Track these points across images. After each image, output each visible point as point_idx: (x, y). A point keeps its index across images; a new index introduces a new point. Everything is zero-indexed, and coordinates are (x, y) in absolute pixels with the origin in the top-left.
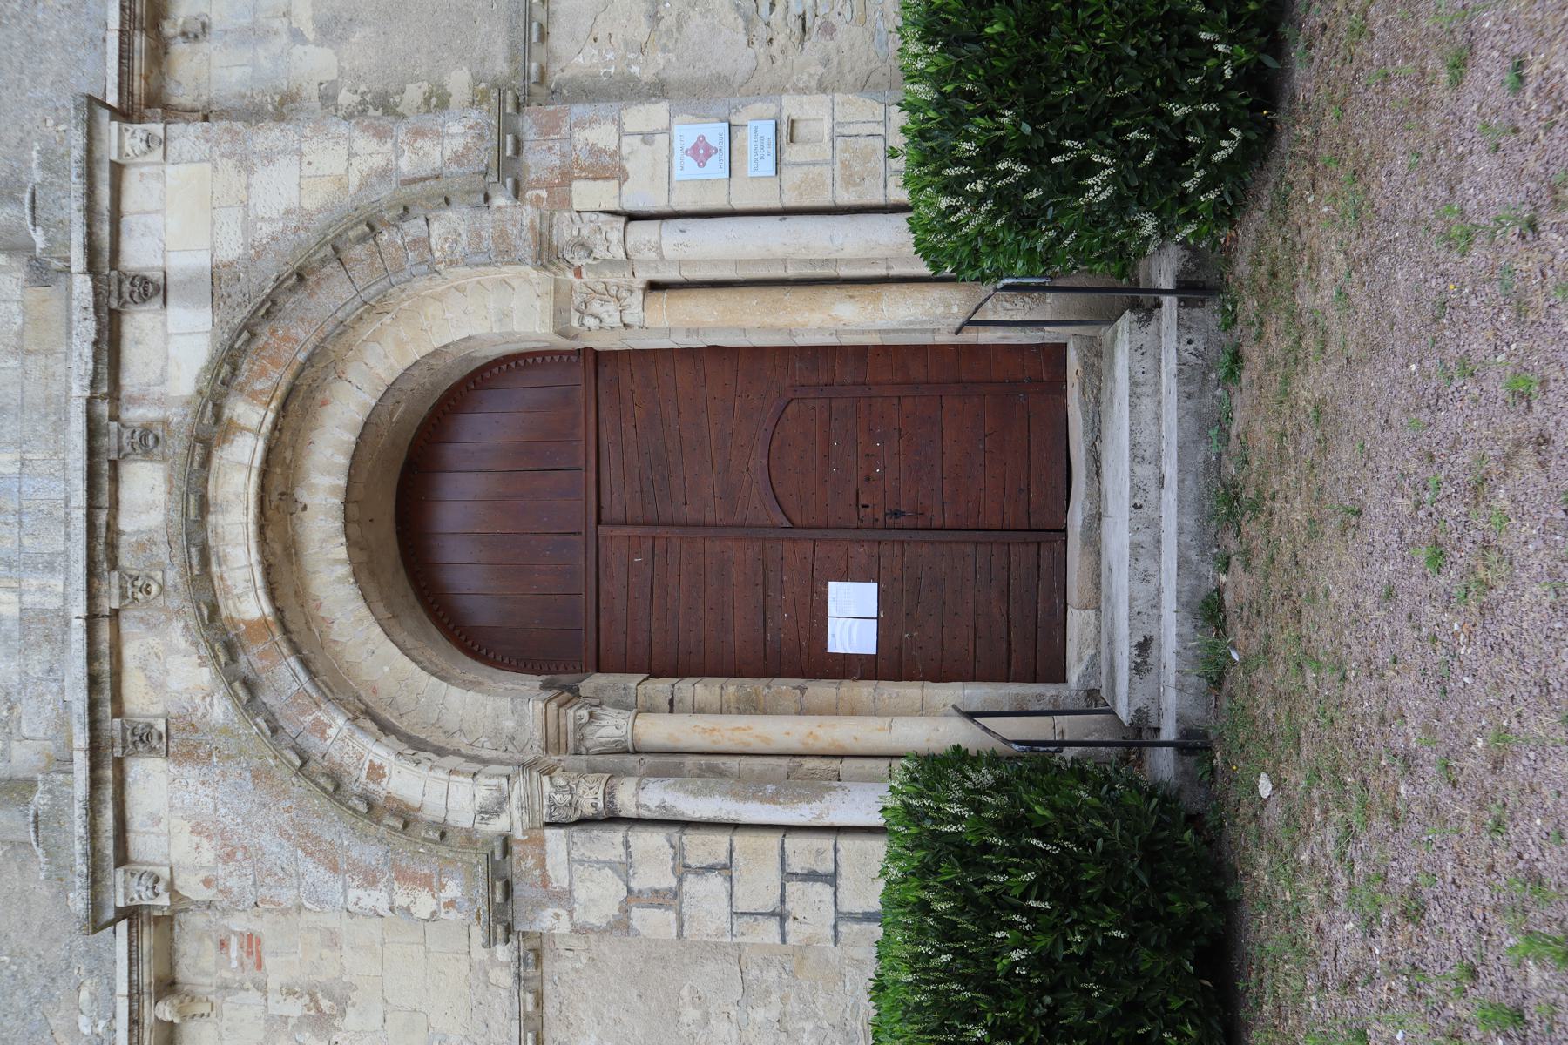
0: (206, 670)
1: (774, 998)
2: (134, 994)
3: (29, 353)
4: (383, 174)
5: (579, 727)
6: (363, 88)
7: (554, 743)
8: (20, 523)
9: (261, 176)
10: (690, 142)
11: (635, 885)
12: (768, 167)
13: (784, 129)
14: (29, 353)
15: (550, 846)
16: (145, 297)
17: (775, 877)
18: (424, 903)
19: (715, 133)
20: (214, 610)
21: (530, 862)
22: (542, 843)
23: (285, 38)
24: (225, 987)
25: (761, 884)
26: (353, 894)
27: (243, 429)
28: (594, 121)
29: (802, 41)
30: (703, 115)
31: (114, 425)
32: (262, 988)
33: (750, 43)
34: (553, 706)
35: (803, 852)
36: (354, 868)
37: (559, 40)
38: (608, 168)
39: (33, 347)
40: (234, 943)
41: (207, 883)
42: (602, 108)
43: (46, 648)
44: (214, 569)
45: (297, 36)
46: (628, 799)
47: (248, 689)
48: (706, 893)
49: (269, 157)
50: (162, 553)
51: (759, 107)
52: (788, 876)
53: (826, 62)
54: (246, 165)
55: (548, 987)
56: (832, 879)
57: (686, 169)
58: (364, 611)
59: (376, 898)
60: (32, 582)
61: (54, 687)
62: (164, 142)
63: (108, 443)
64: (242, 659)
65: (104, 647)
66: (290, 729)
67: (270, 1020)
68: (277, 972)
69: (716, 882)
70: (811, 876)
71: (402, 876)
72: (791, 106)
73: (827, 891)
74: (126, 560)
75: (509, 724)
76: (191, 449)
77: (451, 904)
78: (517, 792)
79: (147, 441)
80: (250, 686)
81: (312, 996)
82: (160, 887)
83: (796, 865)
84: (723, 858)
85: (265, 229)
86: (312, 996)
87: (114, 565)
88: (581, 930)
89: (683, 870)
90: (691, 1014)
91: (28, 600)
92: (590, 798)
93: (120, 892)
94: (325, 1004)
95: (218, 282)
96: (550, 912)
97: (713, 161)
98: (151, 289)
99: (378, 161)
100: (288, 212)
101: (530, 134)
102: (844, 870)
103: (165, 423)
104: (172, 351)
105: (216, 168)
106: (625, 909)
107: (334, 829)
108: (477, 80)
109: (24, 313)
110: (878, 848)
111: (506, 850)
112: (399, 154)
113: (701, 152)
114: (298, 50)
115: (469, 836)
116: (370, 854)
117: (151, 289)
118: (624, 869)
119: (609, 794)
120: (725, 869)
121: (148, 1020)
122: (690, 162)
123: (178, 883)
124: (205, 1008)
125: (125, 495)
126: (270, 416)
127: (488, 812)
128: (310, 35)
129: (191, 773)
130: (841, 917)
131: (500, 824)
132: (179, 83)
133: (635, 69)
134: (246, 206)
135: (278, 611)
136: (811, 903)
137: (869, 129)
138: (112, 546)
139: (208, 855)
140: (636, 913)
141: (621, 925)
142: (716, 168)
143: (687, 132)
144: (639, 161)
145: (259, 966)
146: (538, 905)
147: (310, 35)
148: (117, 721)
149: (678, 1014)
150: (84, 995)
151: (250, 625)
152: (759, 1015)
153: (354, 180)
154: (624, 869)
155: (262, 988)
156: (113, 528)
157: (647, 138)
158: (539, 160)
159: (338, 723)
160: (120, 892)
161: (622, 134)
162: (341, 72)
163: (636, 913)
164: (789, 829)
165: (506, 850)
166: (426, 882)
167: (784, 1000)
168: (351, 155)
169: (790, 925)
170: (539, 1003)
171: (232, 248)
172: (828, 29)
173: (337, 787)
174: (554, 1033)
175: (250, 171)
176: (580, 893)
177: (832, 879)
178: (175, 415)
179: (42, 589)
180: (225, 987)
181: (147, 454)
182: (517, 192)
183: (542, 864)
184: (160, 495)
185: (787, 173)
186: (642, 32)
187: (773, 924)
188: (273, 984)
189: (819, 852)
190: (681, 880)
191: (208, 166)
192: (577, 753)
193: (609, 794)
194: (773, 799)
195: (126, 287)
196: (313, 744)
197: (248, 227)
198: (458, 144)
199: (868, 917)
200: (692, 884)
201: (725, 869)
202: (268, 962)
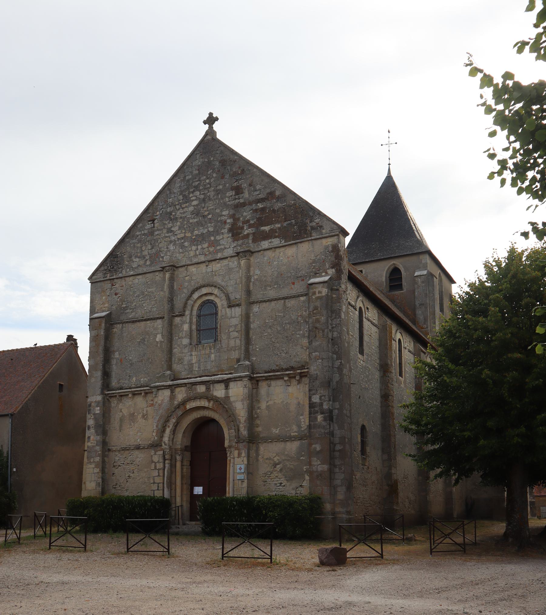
0: (180, 400)
1: (148, 481)
2: (144, 390)
3: (227, 360)
4: (240, 422)
5: (178, 453)
6: (260, 414)
7: (176, 450)
8: (204, 362)
9: (241, 403)
10: (242, 467)
11: (157, 463)
12: (238, 478)
13: (243, 480)
14: (227, 360)
15: (161, 452)
16: (225, 387)
17: (158, 482)
18: (154, 434)
19: (243, 471)
20: (187, 401)
21: (159, 449)
22: (161, 451)
23: (267, 400)
24: (147, 401)
25: (158, 480)
26: (155, 424)
27: (209, 403)
28: (245, 453)
29: (263, 481)
30: (245, 469)
31: (209, 384)
32: (147, 407)
33: (263, 474)
34: (180, 449)
35: (161, 485)
36: (158, 424)
37: (265, 444)
38: (239, 455)
39: (228, 361)
40: (152, 402)
41: (156, 402)
42: (247, 454)
43: (188, 368)
44: (193, 400)
45: (267, 402)
46: (167, 462)
47: (178, 407)
48: (156, 473)
49: (243, 404)
50: (194, 392)
51: (246, 477)
52: (158, 484)
53: (260, 485)
54: (242, 400)
55: (148, 450)
56: (158, 489)
57: (238, 467)
58: (191, 420)
59: (155, 428)
60: (197, 365)
61: (183, 370)
62: (245, 387)
63: (207, 383)
64: (182, 406)
65: (182, 385)
66: (174, 414)
67: (143, 408)
68: (149, 409)
69: (157, 474)
70: (158, 487)
71: (157, 431)
72: (246, 481)
73: (157, 489)
74: (193, 387)
75: (178, 443)
76: (206, 396)
77: (154, 438)
78: (167, 447)
79: (208, 389)
80: (178, 407)
81: (146, 415)
82: (155, 396)
83: (159, 485)
84: (160, 475)
85: (234, 404)
86: (146, 415)
87: (192, 385)
88: (152, 456)
89: (159, 470)
90: (146, 470)
91: (195, 364)
92: (167, 457)
93: (154, 390)
94: (145, 417)
95: (227, 397)
96: (154, 452)
97: (239, 470)
98: (227, 387)
99: (242, 421)
100: (236, 407)
101: (244, 444)
102: (159, 491)
103: (210, 391)
104: (219, 391)
105: (242, 395)
106: (154, 462)
107: (162, 421)
108: (260, 432)
109: (233, 358)
110: (162, 495)
111: (160, 446)
112: (242, 424)
113: (240, 469)
114: (266, 402)
115: (162, 440)
116: (160, 426)
117: (227, 387)
118: (158, 462)
119: (167, 459)
120: (159, 476)
121: (142, 392)
122: (239, 467)
123: (156, 398)
124: (144, 399)
125: (201, 386)
126: (210, 407)
127: (164, 443)
128: (267, 404)
129: (168, 399)
130: (154, 490)
131: (163, 445)
132: (262, 383)
133: (260, 456)
134: (237, 401)
135: (187, 410)
136: (155, 487)
137: (243, 492)
138: (195, 385)
139: (159, 402)
140: (154, 463)
141: (153, 462)
142: (238, 471)
143: (243, 467)
144: (240, 460)
145: (150, 406)
146: (154, 450)
147: (267, 404)
148: (174, 388)
149: (146, 468)
150: (146, 379)
151: (186, 406)
152: (146, 479)
153: (239, 418)
154: (158, 462)
155: (147, 407)
156: (197, 385)
157: (243, 461)
158: (241, 445)
159: (174, 421)
160: (154, 390)
161: (243, 457)
162: (262, 410)
163: (154, 463)
164: (164, 483)
165: (160, 446)
166: (157, 435)
167: (148, 483)
168: (243, 417)
169: (153, 484)
170: (146, 448)
171: (232, 399)
172: (265, 485)
173: (167, 421)
174: (530, 2)
175: (241, 401)
176: (156, 456)
177: (158, 489)
178: (211, 392)
179: (196, 367)
180: (147, 401)
181: (206, 389)
182: (236, 443)
183: (159, 451)
184: (202, 391)
185: (238, 481)
186: (265, 457)
187: (153, 482)
188: (148, 408)
189: (161, 488)
190: (157, 470)
191: (242, 394)
192: (175, 453)
193: (167, 459)
194: (167, 481)
195: (227, 384)
196: (172, 417)
197: (234, 402)
198: (243, 433)
199: (154, 494)
200: (157, 471)
201: (159, 476)
202: (150, 407)
